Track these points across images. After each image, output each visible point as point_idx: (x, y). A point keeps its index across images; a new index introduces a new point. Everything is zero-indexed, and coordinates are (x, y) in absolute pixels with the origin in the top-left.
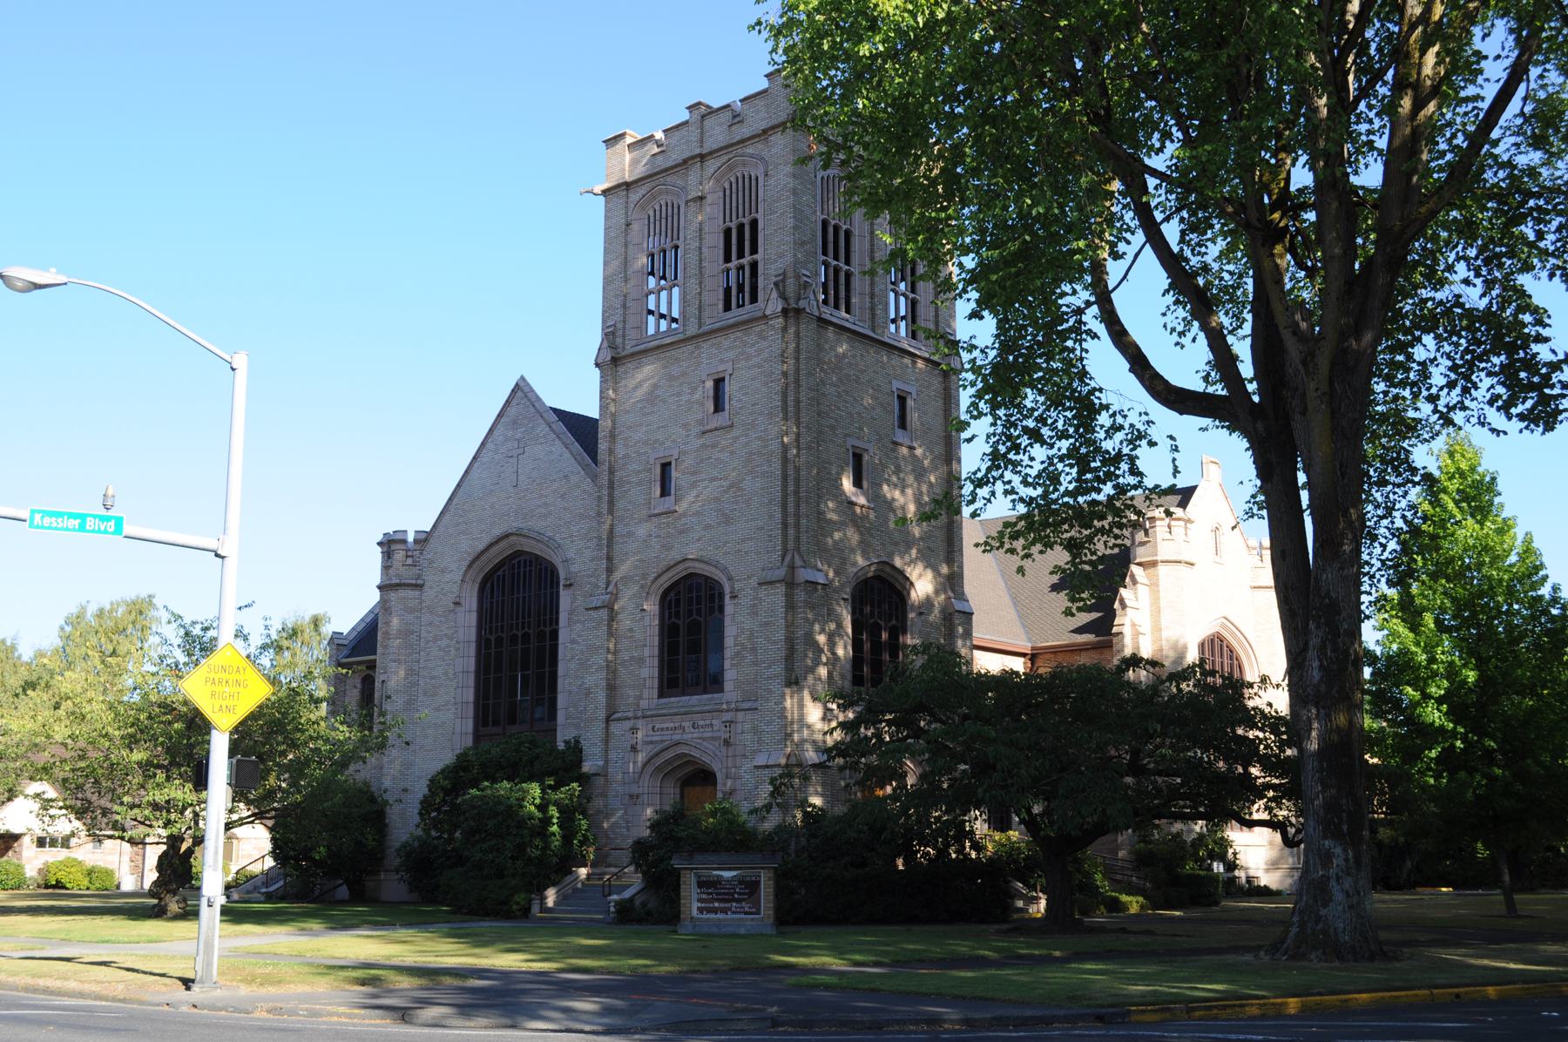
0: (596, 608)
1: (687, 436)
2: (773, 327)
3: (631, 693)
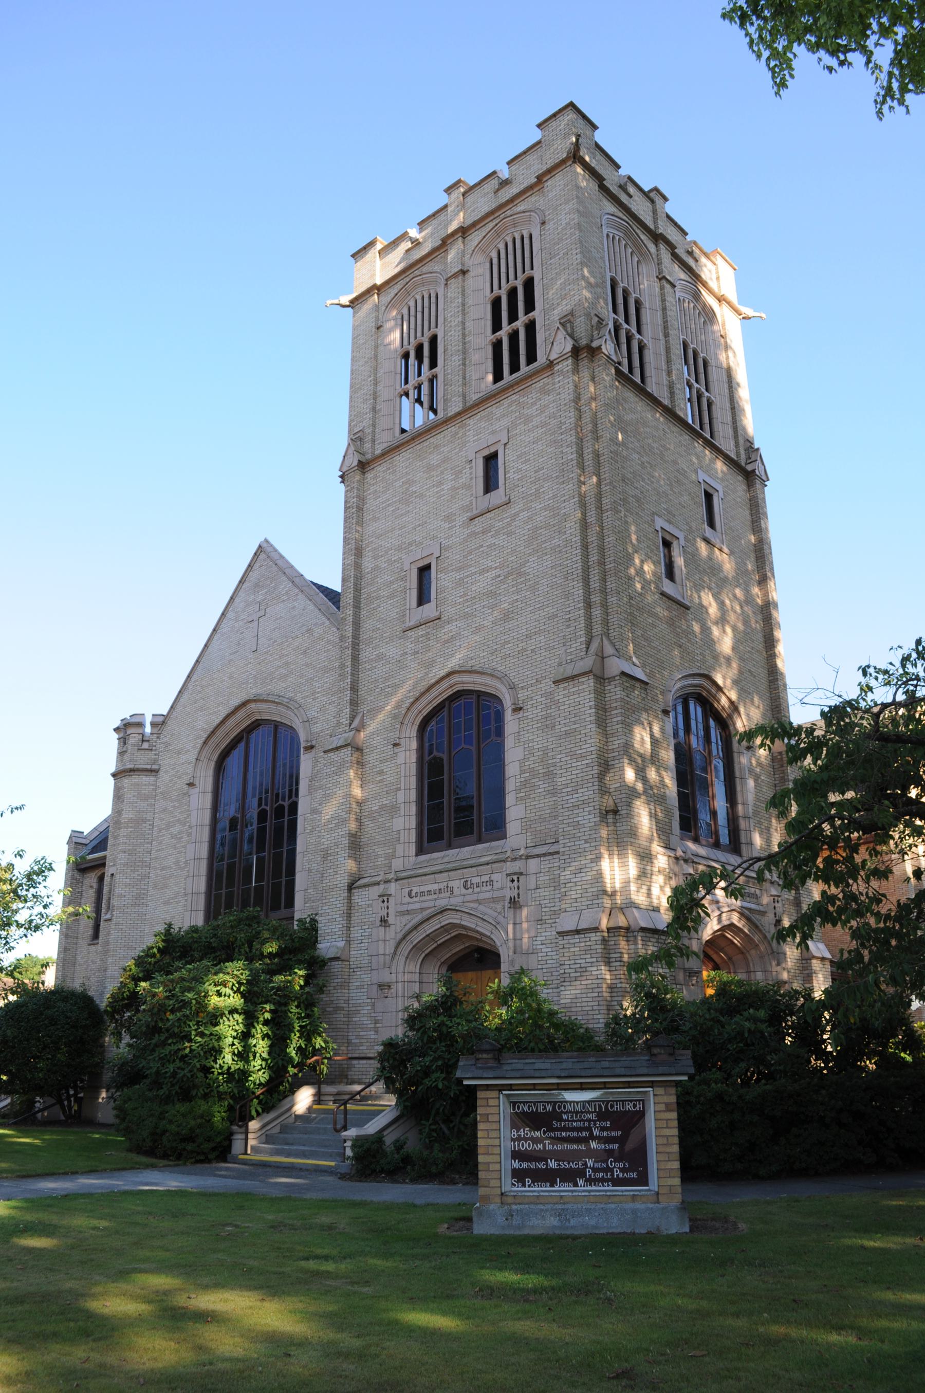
0: (337, 749)
1: (451, 528)
2: (561, 372)
3: (380, 851)
